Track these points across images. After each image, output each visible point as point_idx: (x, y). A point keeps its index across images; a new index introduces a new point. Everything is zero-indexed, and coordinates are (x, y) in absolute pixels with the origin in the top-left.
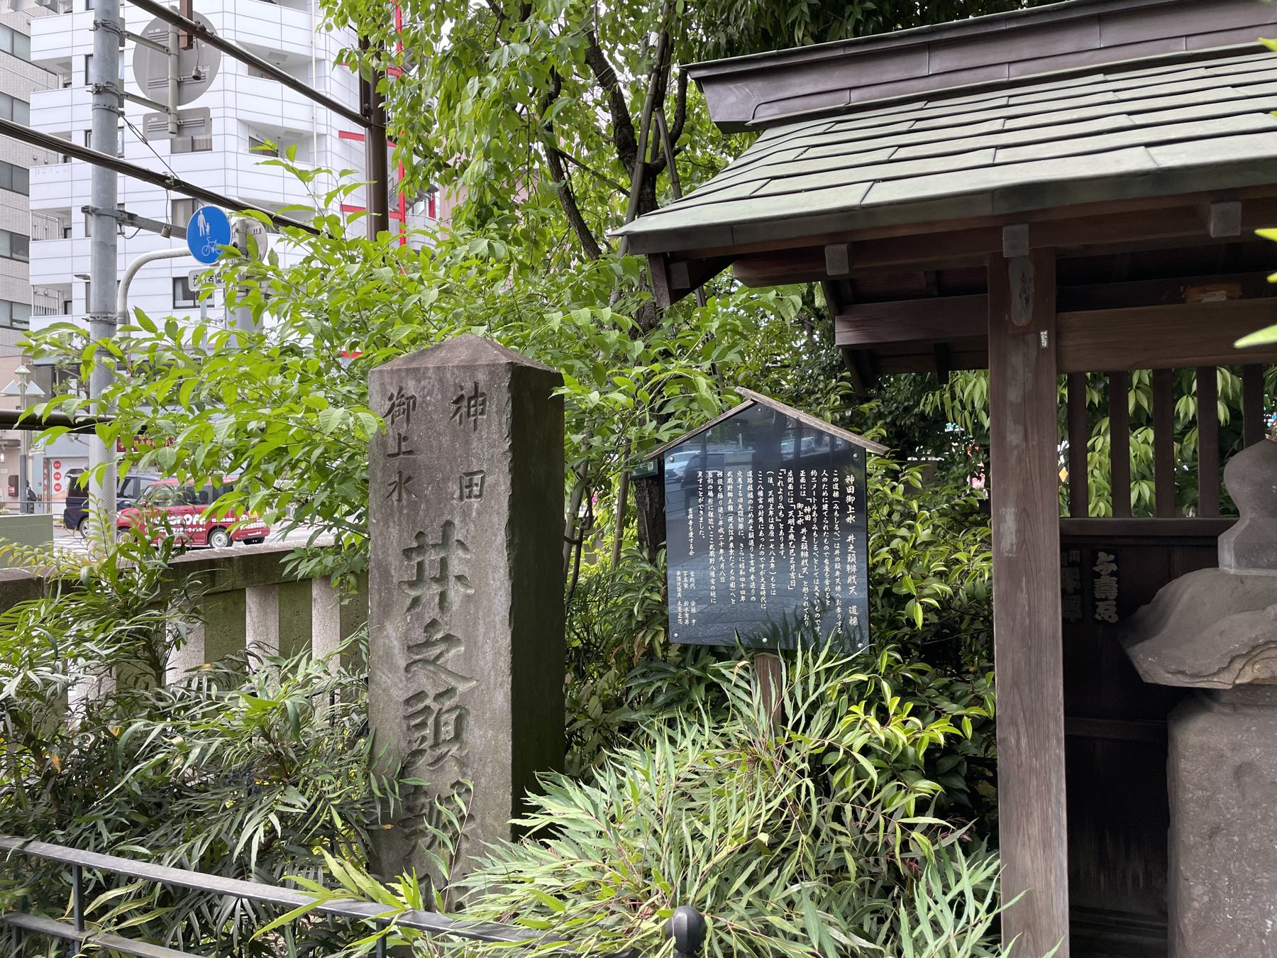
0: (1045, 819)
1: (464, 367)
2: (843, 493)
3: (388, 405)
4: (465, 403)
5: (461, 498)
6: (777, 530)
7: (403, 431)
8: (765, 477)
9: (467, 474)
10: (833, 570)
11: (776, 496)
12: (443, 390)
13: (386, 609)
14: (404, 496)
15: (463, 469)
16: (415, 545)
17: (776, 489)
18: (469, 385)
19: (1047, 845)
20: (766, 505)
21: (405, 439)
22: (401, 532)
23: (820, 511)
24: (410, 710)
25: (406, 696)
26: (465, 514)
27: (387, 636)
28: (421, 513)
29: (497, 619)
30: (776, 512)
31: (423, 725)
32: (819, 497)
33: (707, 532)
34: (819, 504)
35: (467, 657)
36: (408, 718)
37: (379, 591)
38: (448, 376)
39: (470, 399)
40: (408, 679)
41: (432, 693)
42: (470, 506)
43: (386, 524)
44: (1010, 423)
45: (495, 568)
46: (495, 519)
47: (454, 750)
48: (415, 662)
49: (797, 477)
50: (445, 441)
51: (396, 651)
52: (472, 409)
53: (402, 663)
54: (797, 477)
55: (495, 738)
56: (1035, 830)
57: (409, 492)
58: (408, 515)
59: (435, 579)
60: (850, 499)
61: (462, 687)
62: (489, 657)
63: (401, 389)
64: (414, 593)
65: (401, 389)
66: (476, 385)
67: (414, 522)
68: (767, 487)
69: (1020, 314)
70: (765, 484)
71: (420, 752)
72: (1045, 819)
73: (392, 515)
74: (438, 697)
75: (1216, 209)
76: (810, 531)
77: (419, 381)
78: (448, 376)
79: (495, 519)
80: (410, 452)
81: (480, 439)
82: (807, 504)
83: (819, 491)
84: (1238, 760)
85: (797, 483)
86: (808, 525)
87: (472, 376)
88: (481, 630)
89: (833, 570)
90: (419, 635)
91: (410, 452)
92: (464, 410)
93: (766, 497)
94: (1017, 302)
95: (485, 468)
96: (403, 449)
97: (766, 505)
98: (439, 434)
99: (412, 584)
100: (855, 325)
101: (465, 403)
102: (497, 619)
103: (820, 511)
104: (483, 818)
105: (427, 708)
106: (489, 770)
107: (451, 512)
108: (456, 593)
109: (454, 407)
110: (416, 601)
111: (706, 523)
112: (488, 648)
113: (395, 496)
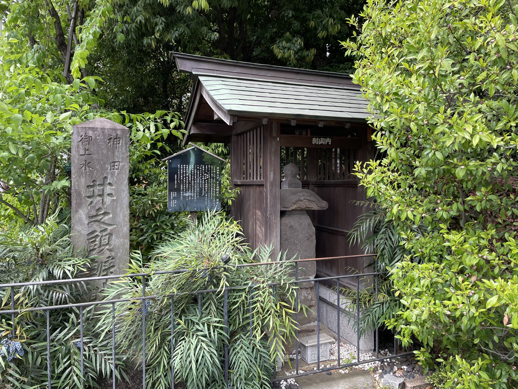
0: (276, 232)
1: (112, 129)
2: (216, 172)
3: (80, 139)
4: (112, 140)
5: (111, 169)
6: (199, 181)
7: (87, 148)
8: (197, 167)
9: (113, 162)
10: (213, 190)
11: (200, 172)
12: (104, 135)
13: (79, 205)
14: (87, 168)
15: (111, 161)
16: (92, 184)
17: (200, 170)
18: (114, 134)
19: (277, 237)
20: (197, 174)
21: (88, 150)
22: (86, 180)
23: (210, 176)
24: (90, 237)
25: (88, 233)
26: (113, 175)
27: (80, 214)
28: (95, 174)
29: (125, 206)
30: (200, 176)
31: (95, 241)
32: (210, 172)
33: (180, 181)
34: (210, 174)
35: (113, 218)
36: (88, 239)
37: (76, 200)
38: (106, 131)
39: (114, 139)
40: (89, 227)
41: (99, 230)
42: (114, 172)
43: (79, 177)
44: (272, 155)
45: (124, 191)
46: (124, 176)
47: (107, 247)
48: (92, 221)
49: (205, 167)
50: (105, 152)
51: (84, 218)
52: (115, 143)
53: (87, 222)
54: (205, 167)
55: (124, 241)
56: (275, 235)
57: (89, 167)
58: (89, 175)
59: (99, 195)
60: (218, 173)
61: (110, 228)
62: (121, 217)
63: (86, 133)
64: (90, 200)
65: (86, 133)
66: (117, 135)
67: (92, 177)
68: (197, 169)
69: (274, 134)
70: (197, 168)
71: (93, 250)
72: (276, 232)
73: (82, 174)
74: (101, 231)
75: (321, 122)
76: (208, 181)
77: (94, 132)
78: (106, 131)
79: (124, 176)
80: (90, 154)
81: (118, 152)
82: (207, 174)
83: (210, 170)
84: (289, 225)
85: (205, 168)
86: (208, 179)
87: (115, 132)
88: (119, 209)
89: (213, 190)
90: (94, 213)
91: (90, 154)
92: (112, 143)
93: (197, 172)
94: (274, 132)
95: (120, 160)
96: (87, 153)
97: (197, 174)
98: (102, 149)
99: (89, 197)
100: (197, 128)
101: (112, 140)
102: (125, 206)
103: (210, 176)
104: (119, 266)
105: (97, 235)
106: (121, 251)
107: (107, 174)
108: (108, 200)
109: (108, 141)
110: (91, 202)
111: (180, 179)
112: (121, 215)
113: (83, 168)
